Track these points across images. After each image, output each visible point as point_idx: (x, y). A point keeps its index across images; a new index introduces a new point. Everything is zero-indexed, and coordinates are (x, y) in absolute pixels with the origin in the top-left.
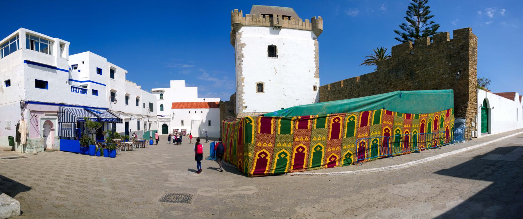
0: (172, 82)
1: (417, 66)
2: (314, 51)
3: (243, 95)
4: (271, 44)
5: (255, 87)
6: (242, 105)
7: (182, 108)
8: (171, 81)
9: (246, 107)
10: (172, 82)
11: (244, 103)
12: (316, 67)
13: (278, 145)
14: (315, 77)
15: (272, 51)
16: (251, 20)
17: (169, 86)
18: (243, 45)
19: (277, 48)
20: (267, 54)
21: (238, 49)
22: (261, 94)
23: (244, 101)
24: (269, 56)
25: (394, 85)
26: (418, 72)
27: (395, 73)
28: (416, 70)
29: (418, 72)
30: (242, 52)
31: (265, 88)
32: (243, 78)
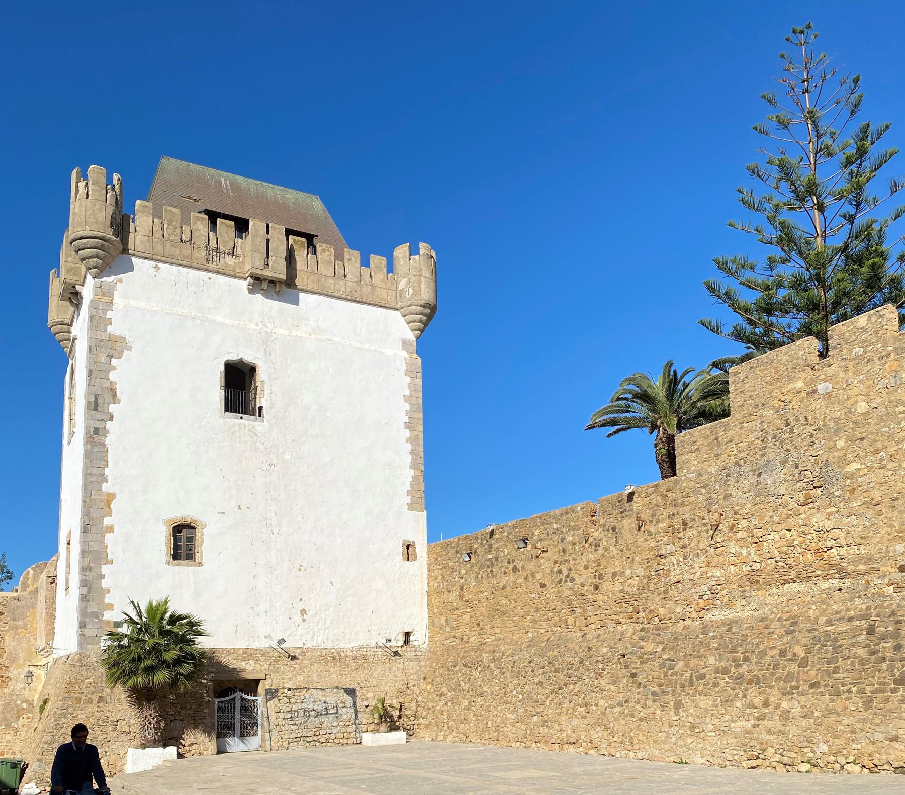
1: (850, 440)
2: (406, 399)
3: (105, 569)
11: (111, 607)
12: (413, 466)
14: (411, 507)
20: (217, 395)
24: (227, 410)
25: (748, 529)
26: (855, 466)
27: (753, 479)
28: (844, 461)
29: (855, 466)
30: (112, 376)
31: (162, 539)
32: (110, 498)
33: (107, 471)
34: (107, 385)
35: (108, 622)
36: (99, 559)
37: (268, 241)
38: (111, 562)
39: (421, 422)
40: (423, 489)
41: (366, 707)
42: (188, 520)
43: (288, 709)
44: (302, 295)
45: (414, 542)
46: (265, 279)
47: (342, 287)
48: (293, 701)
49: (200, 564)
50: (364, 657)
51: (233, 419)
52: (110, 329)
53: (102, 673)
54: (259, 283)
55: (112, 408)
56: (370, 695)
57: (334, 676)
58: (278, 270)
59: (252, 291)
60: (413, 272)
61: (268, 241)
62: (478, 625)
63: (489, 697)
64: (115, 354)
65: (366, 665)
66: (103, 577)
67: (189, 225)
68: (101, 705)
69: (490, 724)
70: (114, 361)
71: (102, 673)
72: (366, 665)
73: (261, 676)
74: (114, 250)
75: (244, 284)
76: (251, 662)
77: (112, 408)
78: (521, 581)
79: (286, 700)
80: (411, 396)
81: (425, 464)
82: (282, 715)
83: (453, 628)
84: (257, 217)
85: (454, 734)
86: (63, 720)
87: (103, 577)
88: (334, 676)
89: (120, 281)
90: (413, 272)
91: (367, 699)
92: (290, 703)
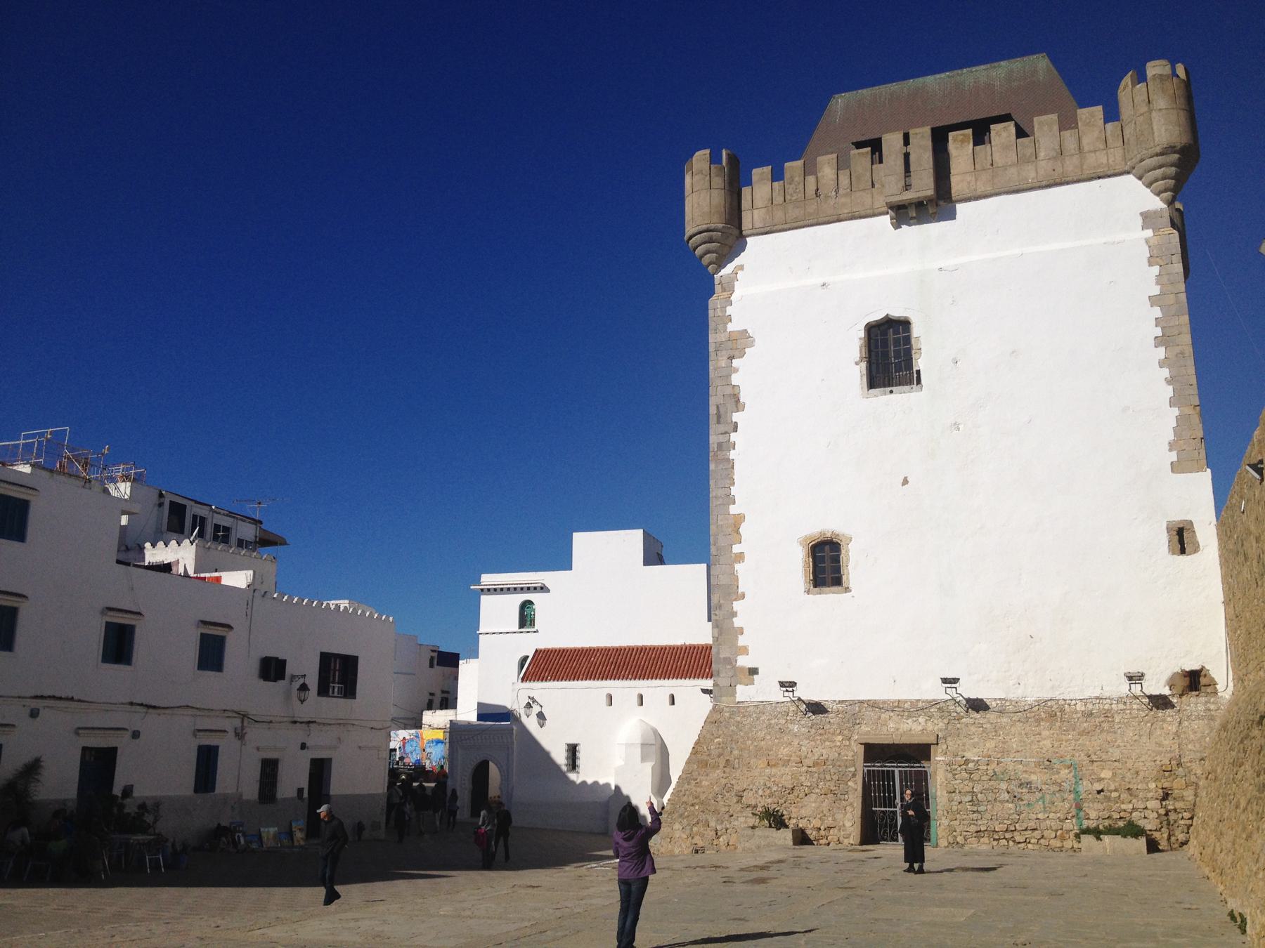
0: (581, 540)
2: (1153, 300)
3: (737, 606)
4: (878, 316)
5: (797, 563)
6: (730, 662)
7: (575, 676)
8: (575, 535)
9: (753, 671)
10: (581, 540)
11: (745, 650)
13: (273, 830)
15: (889, 354)
16: (779, 199)
17: (563, 561)
18: (740, 343)
19: (916, 331)
20: (857, 372)
21: (717, 363)
22: (828, 599)
23: (742, 641)
31: (854, 564)
32: (740, 519)
34: (728, 391)
35: (742, 669)
36: (729, 594)
38: (743, 596)
39: (1187, 329)
40: (1200, 434)
41: (1099, 792)
42: (829, 535)
43: (968, 789)
44: (959, 206)
45: (1191, 523)
46: (911, 204)
47: (1044, 166)
48: (975, 777)
49: (847, 590)
50: (1108, 715)
53: (855, 754)
54: (904, 213)
55: (736, 417)
56: (1106, 774)
58: (924, 185)
59: (897, 225)
60: (1153, 105)
61: (907, 156)
64: (737, 353)
65: (1105, 725)
66: (734, 614)
68: (727, 770)
70: (736, 362)
71: (855, 754)
72: (1105, 725)
73: (932, 740)
74: (731, 239)
75: (886, 220)
76: (921, 720)
77: (736, 417)
79: (966, 775)
80: (1162, 294)
81: (1200, 395)
82: (957, 797)
84: (889, 131)
87: (734, 614)
88: (1047, 743)
89: (741, 267)
90: (1153, 105)
91: (1100, 780)
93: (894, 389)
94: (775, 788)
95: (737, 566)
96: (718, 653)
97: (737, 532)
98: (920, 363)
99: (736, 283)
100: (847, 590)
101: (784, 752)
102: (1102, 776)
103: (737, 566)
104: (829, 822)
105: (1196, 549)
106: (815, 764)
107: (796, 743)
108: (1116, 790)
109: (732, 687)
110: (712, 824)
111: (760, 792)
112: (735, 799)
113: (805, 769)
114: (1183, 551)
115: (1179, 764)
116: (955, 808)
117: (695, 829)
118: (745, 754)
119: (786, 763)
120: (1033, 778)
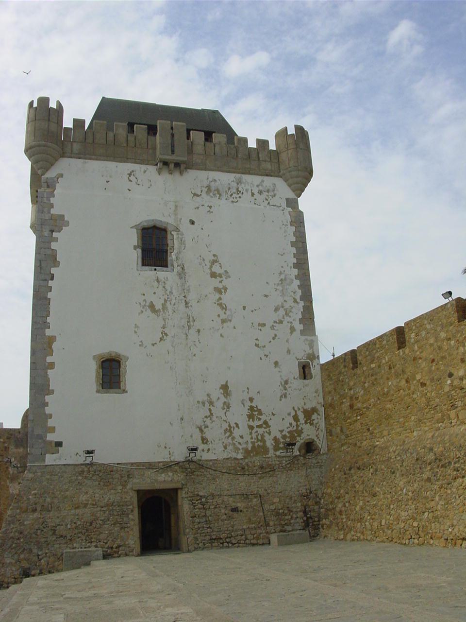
3: (48, 398)
6: (41, 437)
9: (59, 444)
11: (53, 430)
15: (155, 246)
22: (111, 397)
23: (51, 423)
24: (143, 265)
31: (131, 375)
33: (49, 320)
35: (51, 442)
37: (173, 135)
38: (53, 391)
42: (113, 355)
43: (203, 514)
48: (206, 506)
49: (124, 391)
51: (150, 273)
52: (53, 211)
55: (53, 270)
56: (276, 500)
57: (243, 484)
62: (368, 430)
63: (382, 496)
66: (47, 404)
67: (113, 131)
69: (383, 523)
70: (55, 235)
71: (132, 497)
77: (53, 270)
78: (403, 382)
79: (200, 506)
83: (347, 436)
85: (352, 533)
86: (12, 526)
87: (47, 404)
91: (273, 503)
92: (204, 508)
93: (157, 268)
94: (79, 523)
95: (49, 372)
96: (33, 431)
97: (51, 348)
98: (144, 267)
99: (57, 185)
100: (124, 391)
101: (83, 498)
102: (274, 501)
103: (49, 372)
104: (119, 542)
105: (311, 378)
106: (107, 505)
107: (91, 492)
108: (282, 509)
109: (43, 455)
110: (35, 551)
111: (69, 526)
112: (51, 533)
113: (99, 509)
114: (305, 378)
115: (311, 492)
116: (196, 526)
117: (22, 556)
118: (56, 501)
119: (85, 506)
120: (239, 505)
